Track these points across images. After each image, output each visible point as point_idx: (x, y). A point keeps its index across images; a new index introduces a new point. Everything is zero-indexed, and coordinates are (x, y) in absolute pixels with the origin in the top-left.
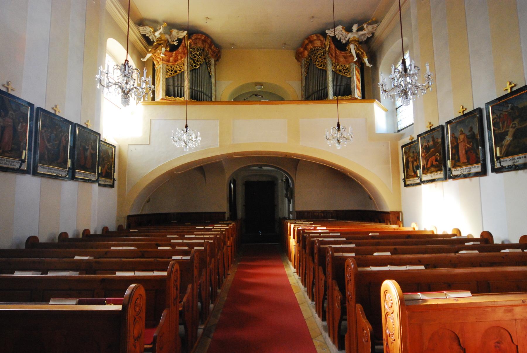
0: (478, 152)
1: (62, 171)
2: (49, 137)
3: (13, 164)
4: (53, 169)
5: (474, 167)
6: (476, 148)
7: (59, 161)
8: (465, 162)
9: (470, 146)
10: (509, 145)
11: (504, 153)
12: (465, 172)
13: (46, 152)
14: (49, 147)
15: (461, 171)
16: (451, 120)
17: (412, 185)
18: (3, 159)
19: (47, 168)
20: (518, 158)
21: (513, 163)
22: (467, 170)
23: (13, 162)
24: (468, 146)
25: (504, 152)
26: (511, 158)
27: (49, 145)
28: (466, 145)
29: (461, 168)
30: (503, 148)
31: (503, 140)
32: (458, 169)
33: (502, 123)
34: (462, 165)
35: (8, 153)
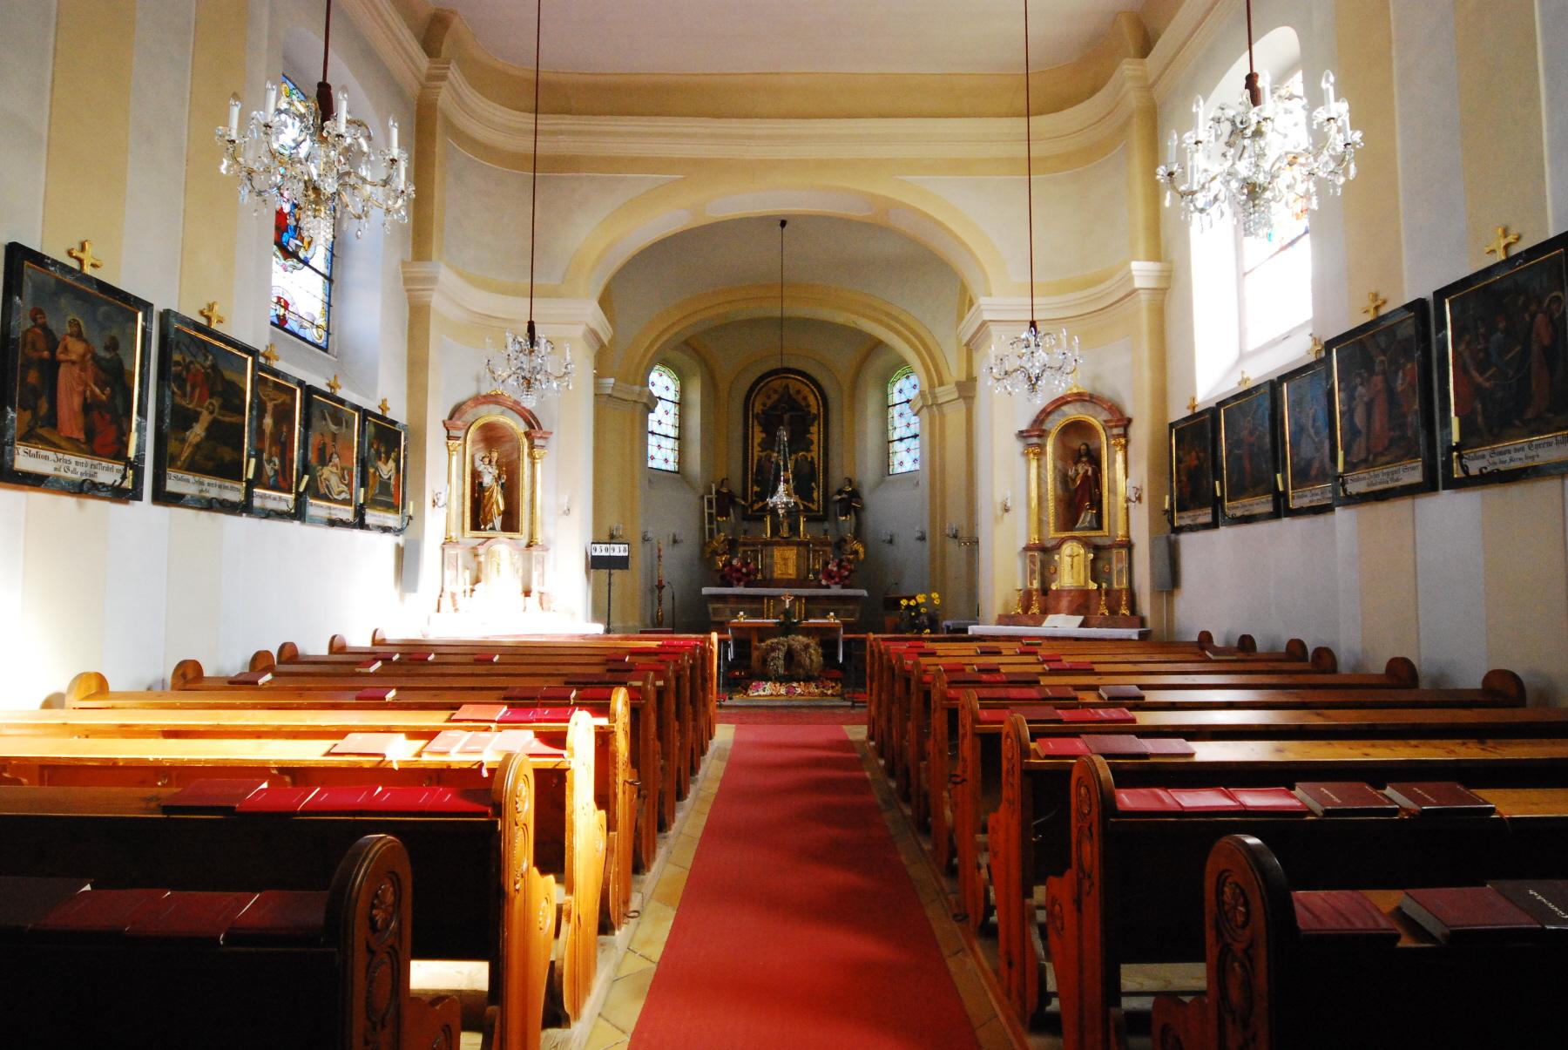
0: (125, 426)
1: (1550, 444)
2: (1481, 355)
3: (1395, 476)
4: (1509, 452)
5: (108, 469)
6: (121, 412)
7: (1529, 414)
8: (78, 440)
9: (104, 397)
10: (197, 446)
11: (185, 460)
12: (74, 472)
13: (1479, 406)
14: (1487, 385)
15: (57, 465)
16: (49, 258)
17: (269, 514)
18: (1376, 473)
19: (1526, 447)
20: (209, 484)
21: (201, 491)
22: (80, 469)
23: (1396, 472)
24: (97, 391)
25: (186, 458)
26: (197, 478)
27: (1488, 380)
28: (86, 385)
29: (60, 456)
30: (186, 446)
31: (187, 430)
32: (186, 476)
33: (191, 386)
34: (63, 444)
35: (1384, 455)
